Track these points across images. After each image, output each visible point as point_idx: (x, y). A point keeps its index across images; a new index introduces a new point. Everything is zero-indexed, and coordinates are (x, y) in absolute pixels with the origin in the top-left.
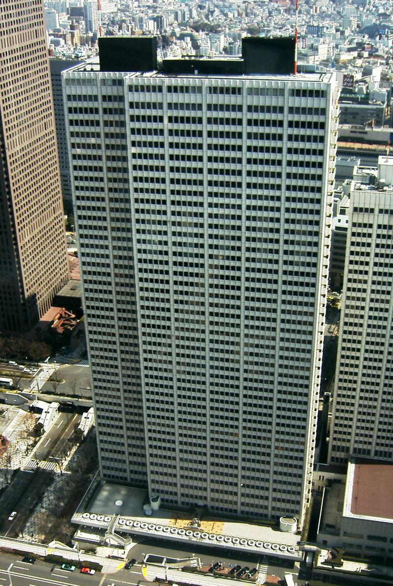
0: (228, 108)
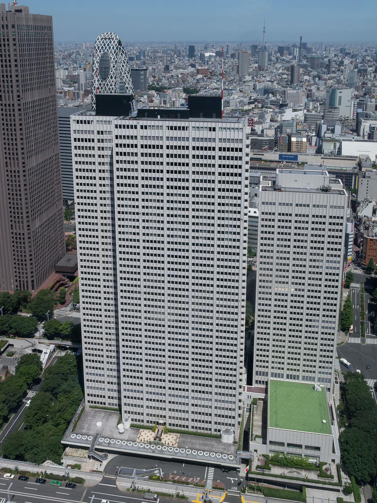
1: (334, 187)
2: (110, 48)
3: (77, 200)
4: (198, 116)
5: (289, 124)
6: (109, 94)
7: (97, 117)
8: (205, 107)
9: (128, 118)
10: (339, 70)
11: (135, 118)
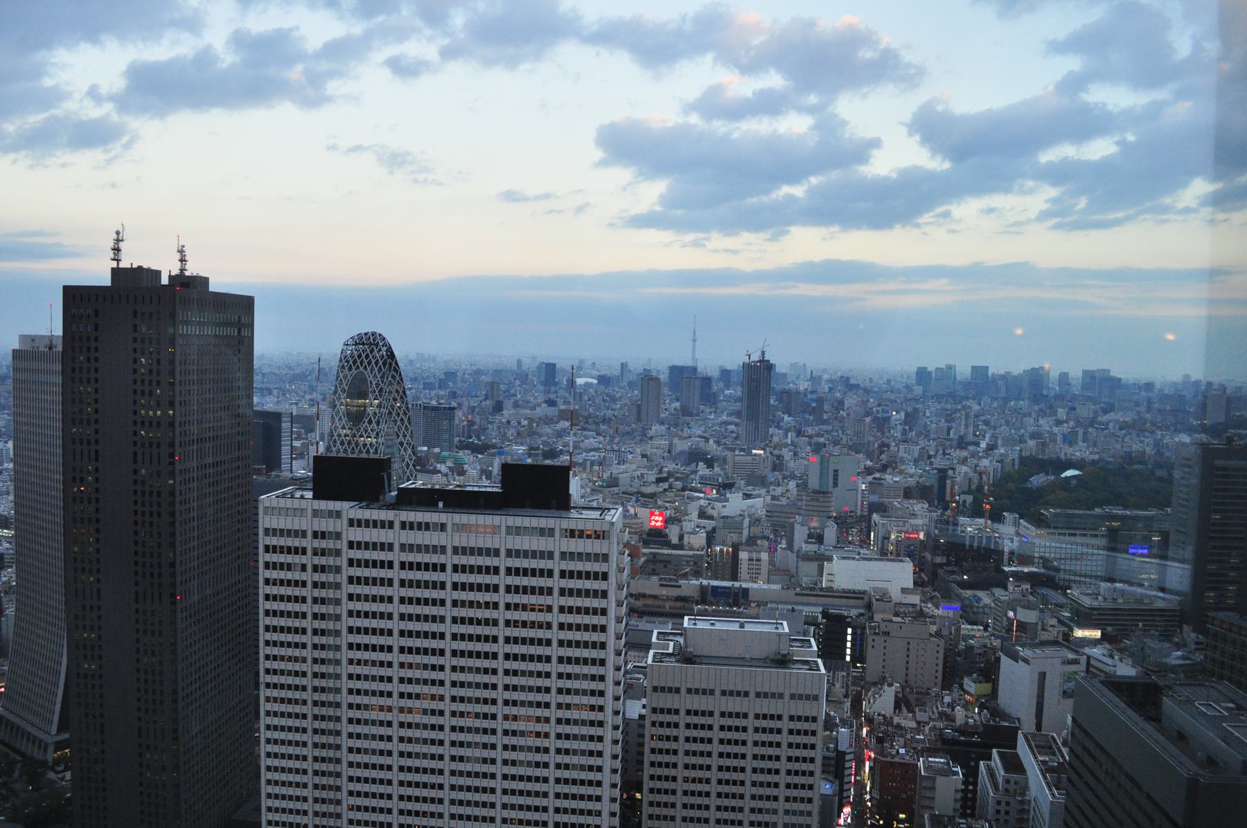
0: (588, 557)
1: (798, 653)
2: (369, 363)
4: (523, 506)
5: (731, 523)
6: (364, 456)
7: (317, 502)
9: (375, 505)
10: (836, 419)
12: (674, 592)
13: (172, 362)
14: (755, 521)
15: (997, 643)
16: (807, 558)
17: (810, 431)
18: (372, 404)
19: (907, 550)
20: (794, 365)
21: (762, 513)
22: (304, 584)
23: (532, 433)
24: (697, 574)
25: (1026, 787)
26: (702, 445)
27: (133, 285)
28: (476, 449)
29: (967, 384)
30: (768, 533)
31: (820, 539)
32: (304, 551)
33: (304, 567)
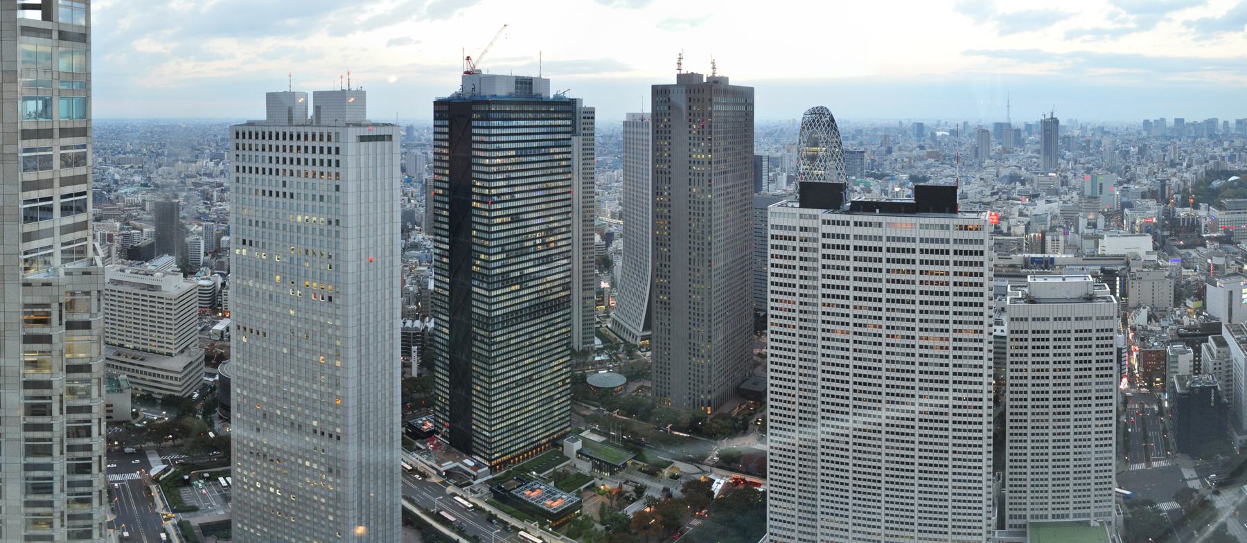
1: (1099, 293)
3: (770, 312)
5: (1040, 219)
8: (935, 200)
11: (847, 212)
12: (1008, 262)
13: (710, 127)
14: (1054, 217)
15: (1203, 278)
16: (1087, 237)
17: (1082, 160)
18: (821, 150)
19: (1147, 229)
20: (1070, 121)
21: (1058, 212)
22: (794, 258)
23: (911, 167)
24: (1020, 250)
25: (1228, 354)
26: (1017, 171)
27: (688, 82)
28: (877, 177)
29: (1172, 129)
30: (1062, 223)
31: (1095, 226)
32: (794, 239)
33: (794, 248)
